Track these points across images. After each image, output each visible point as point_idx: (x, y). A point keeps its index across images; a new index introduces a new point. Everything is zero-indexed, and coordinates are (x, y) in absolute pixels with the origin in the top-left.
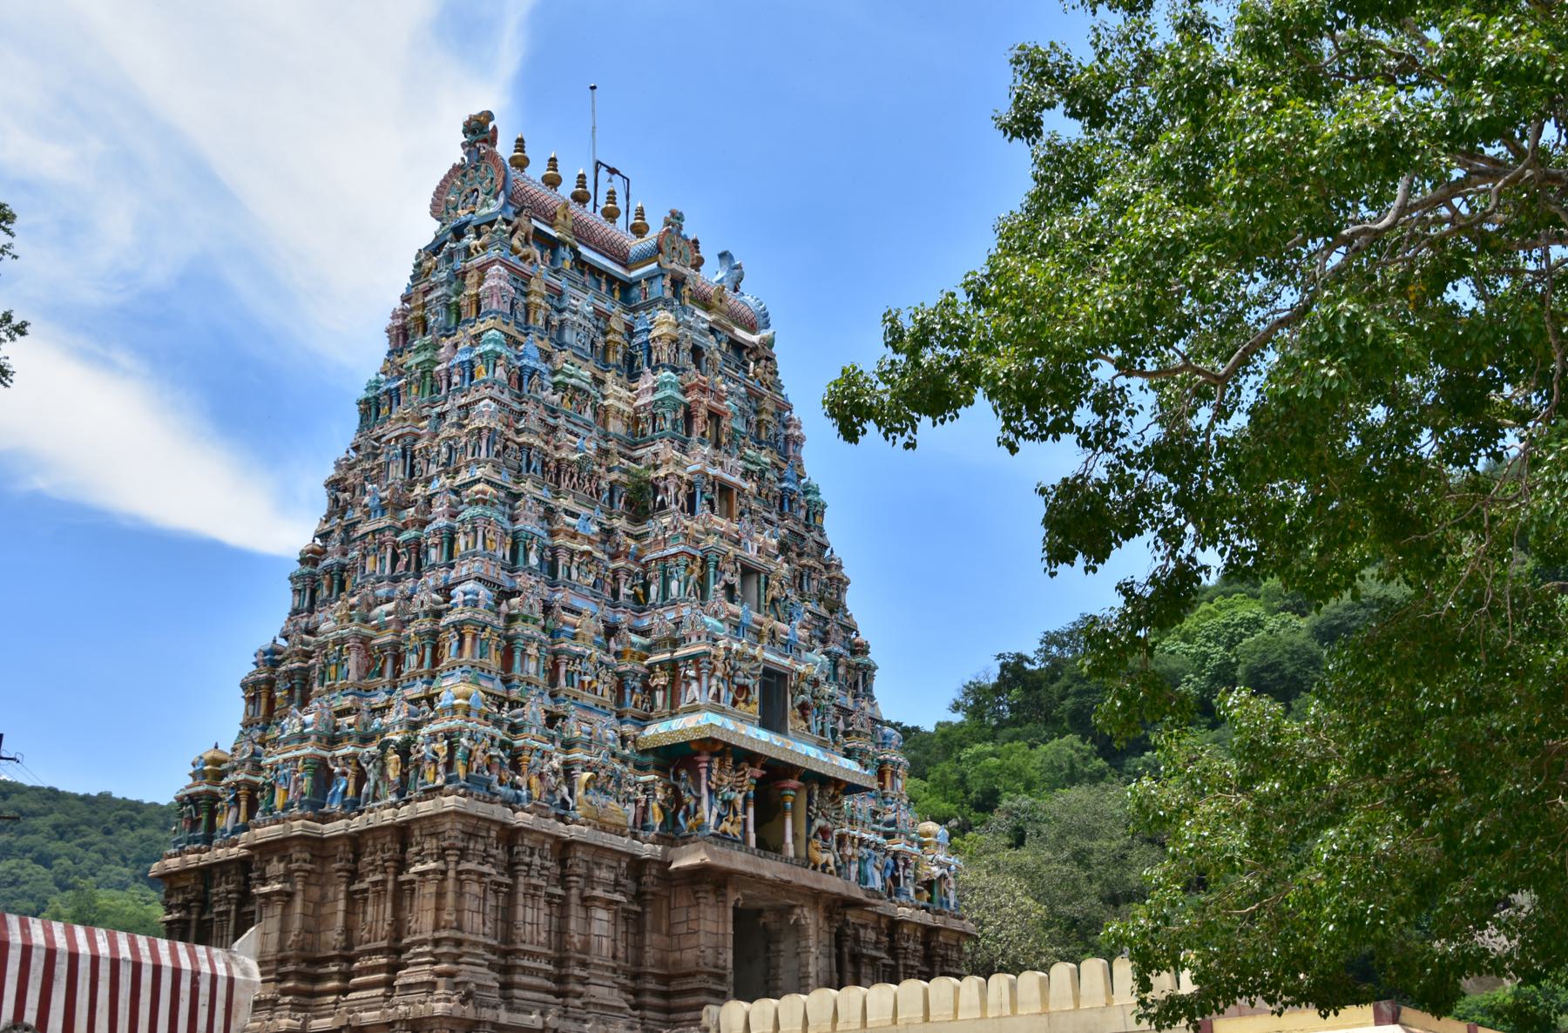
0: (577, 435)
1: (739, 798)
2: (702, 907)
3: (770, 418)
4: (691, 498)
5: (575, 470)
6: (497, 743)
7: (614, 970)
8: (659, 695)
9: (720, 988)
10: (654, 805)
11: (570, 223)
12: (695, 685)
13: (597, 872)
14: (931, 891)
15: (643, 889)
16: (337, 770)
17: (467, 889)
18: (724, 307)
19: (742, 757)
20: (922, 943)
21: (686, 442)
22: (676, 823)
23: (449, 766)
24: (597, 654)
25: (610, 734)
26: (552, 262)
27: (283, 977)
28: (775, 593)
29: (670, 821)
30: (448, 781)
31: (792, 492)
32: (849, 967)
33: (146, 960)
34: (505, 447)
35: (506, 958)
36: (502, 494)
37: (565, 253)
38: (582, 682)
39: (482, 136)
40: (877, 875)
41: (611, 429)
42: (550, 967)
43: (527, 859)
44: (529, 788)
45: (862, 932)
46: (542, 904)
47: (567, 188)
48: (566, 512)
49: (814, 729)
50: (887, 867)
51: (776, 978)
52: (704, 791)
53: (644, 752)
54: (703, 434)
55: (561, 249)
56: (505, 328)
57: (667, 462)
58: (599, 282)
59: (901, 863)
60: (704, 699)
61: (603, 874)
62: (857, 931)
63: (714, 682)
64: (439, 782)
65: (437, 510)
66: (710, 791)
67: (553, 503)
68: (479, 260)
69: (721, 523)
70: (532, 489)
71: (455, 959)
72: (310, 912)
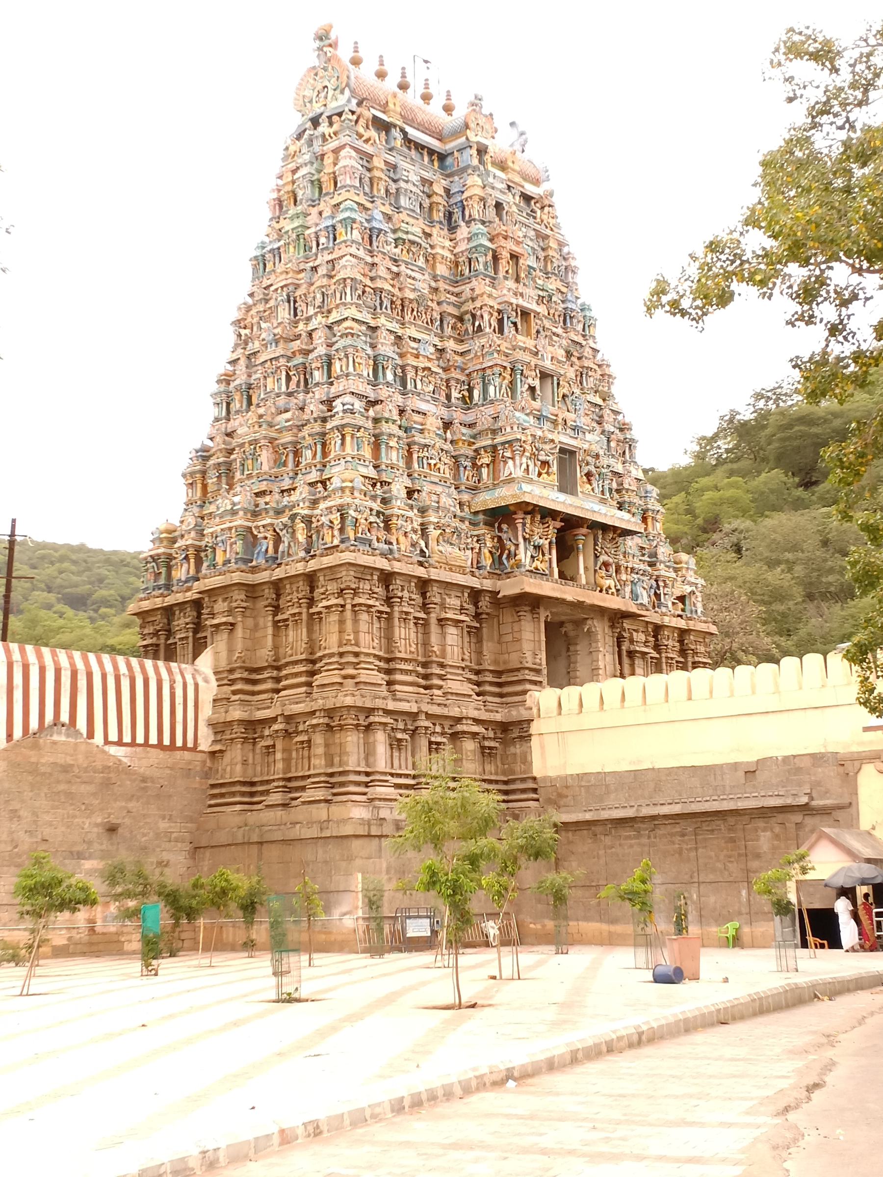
0: (414, 279)
2: (523, 623)
3: (555, 254)
4: (500, 322)
5: (415, 305)
6: (374, 513)
8: (485, 471)
10: (486, 551)
11: (398, 109)
12: (510, 462)
13: (448, 600)
16: (260, 536)
18: (517, 168)
19: (548, 514)
20: (679, 641)
23: (342, 530)
24: (439, 443)
28: (565, 391)
29: (498, 561)
30: (342, 541)
31: (572, 310)
32: (627, 660)
34: (364, 292)
36: (364, 328)
37: (396, 133)
43: (400, 594)
45: (635, 634)
49: (596, 491)
52: (521, 540)
53: (476, 513)
54: (507, 272)
55: (393, 130)
57: (482, 295)
58: (422, 154)
62: (631, 634)
63: (524, 460)
66: (525, 539)
67: (400, 332)
68: (333, 144)
69: (522, 340)
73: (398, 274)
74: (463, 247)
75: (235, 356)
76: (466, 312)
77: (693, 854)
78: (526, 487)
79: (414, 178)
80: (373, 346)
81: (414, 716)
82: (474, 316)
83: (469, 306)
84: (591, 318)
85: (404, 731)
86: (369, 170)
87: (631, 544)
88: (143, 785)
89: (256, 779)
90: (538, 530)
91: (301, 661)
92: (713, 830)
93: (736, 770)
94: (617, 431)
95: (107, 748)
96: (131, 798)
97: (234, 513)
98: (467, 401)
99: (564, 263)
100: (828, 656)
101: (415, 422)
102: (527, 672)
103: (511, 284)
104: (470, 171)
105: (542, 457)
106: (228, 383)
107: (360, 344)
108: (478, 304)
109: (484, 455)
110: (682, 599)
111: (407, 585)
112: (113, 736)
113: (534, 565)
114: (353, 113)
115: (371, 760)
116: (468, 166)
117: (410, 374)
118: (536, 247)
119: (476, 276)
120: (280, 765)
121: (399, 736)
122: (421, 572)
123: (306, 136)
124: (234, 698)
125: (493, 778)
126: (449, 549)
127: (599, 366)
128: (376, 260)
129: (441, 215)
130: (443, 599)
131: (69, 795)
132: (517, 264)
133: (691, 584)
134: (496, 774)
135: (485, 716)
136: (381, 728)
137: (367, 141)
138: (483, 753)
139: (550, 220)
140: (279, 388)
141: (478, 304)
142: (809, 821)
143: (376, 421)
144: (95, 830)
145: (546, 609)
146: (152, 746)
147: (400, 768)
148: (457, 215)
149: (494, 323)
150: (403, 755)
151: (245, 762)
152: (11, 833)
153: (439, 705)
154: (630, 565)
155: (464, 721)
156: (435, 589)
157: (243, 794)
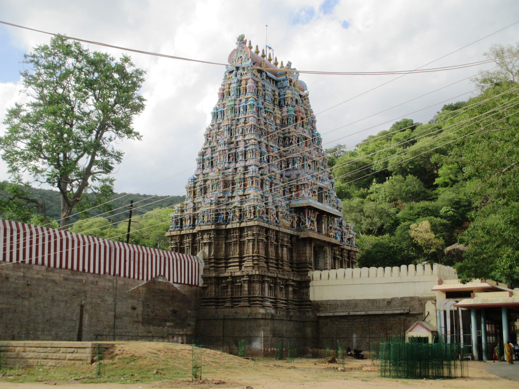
1: (314, 220)
19: (315, 210)
22: (299, 226)
23: (254, 213)
29: (298, 225)
30: (254, 217)
33: (70, 238)
35: (267, 260)
37: (264, 74)
47: (260, 54)
51: (318, 263)
52: (307, 219)
53: (291, 208)
61: (286, 239)
68: (244, 77)
71: (258, 260)
75: (206, 147)
76: (287, 137)
77: (368, 328)
79: (270, 90)
82: (289, 139)
83: (287, 135)
90: (313, 215)
91: (236, 258)
97: (211, 204)
100: (417, 266)
103: (301, 128)
105: (314, 190)
106: (203, 156)
110: (349, 239)
112: (175, 281)
122: (277, 229)
128: (260, 118)
135: (295, 279)
137: (256, 77)
140: (226, 160)
142: (409, 319)
143: (262, 175)
148: (282, 103)
151: (215, 291)
152: (147, 312)
157: (215, 302)
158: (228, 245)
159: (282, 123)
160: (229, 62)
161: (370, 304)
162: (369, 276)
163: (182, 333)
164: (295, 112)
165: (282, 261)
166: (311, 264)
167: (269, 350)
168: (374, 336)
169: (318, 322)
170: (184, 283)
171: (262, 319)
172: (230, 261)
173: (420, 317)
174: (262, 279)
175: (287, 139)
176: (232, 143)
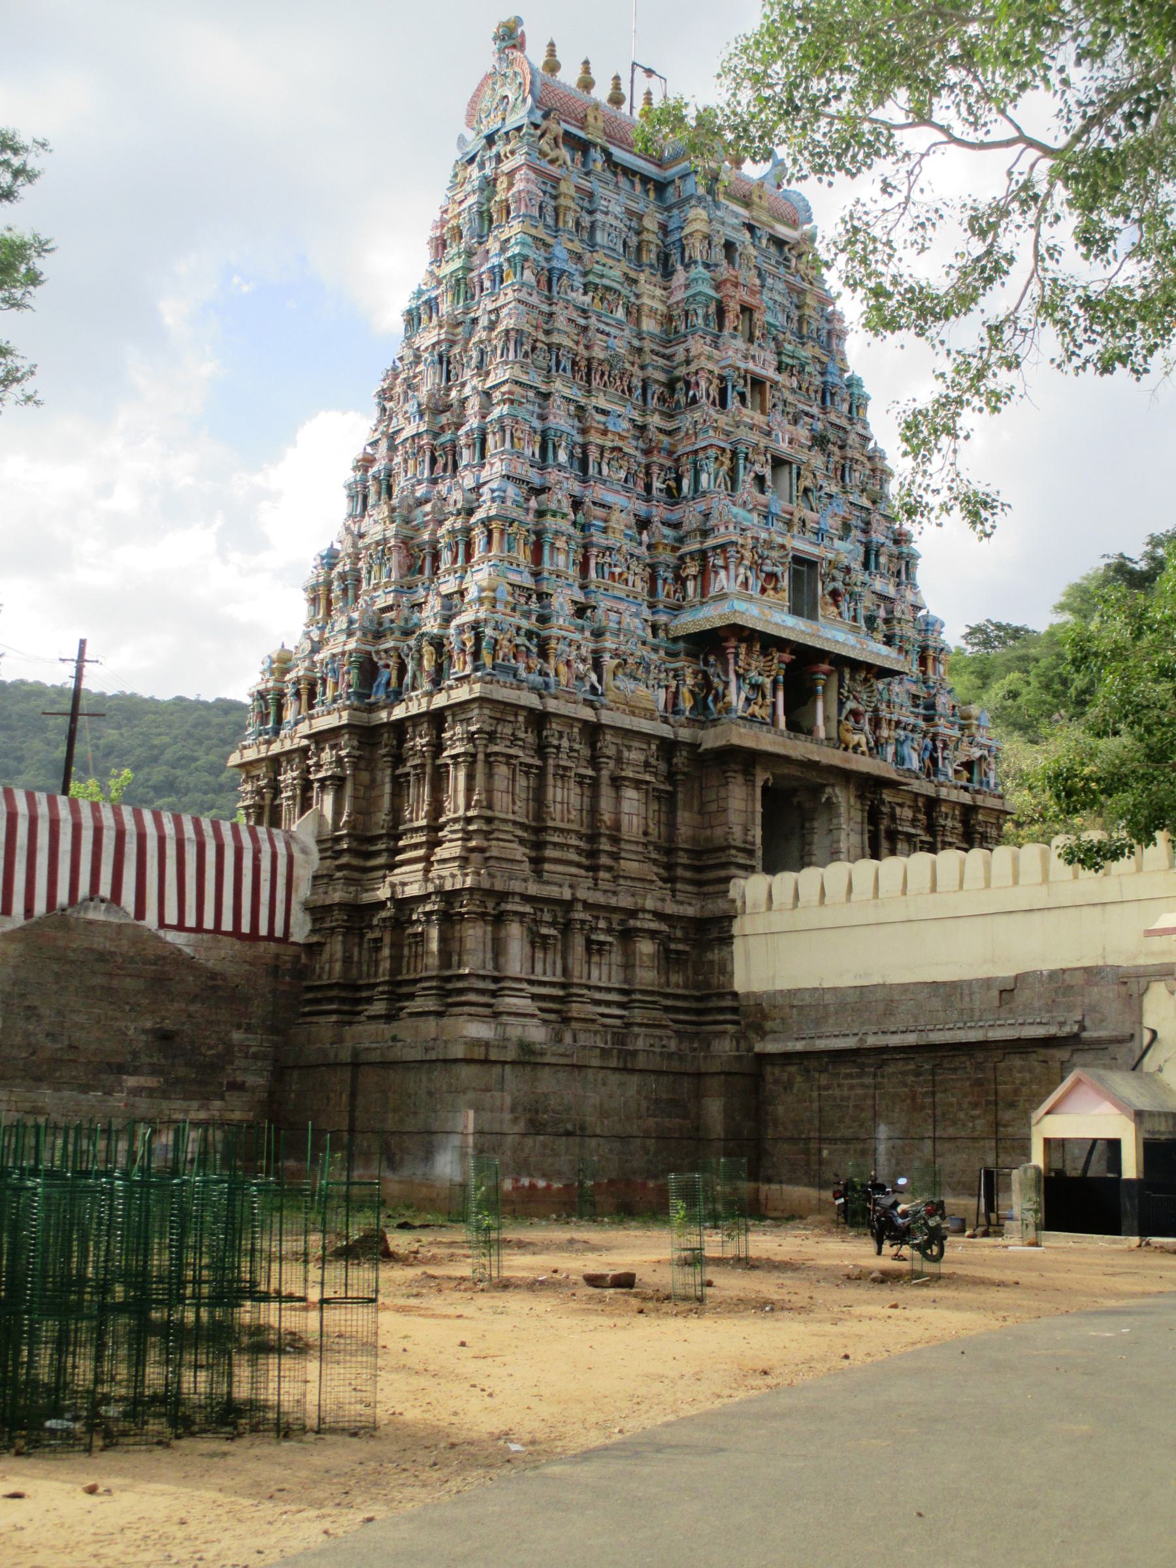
0: (608, 334)
1: (768, 682)
2: (731, 787)
3: (813, 313)
4: (723, 392)
5: (606, 368)
6: (522, 632)
7: (645, 845)
8: (690, 585)
9: (749, 862)
10: (684, 691)
11: (601, 124)
12: (723, 573)
13: (626, 754)
14: (971, 772)
15: (674, 769)
16: (381, 663)
17: (496, 770)
18: (764, 203)
19: (769, 643)
20: (961, 821)
21: (718, 337)
22: (706, 707)
23: (476, 655)
24: (628, 546)
25: (633, 624)
26: (584, 164)
27: (339, 854)
28: (808, 483)
29: (700, 705)
30: (476, 669)
31: (834, 385)
32: (881, 841)
34: (534, 349)
35: (537, 834)
36: (531, 394)
37: (596, 154)
38: (612, 574)
39: (512, 42)
40: (915, 756)
41: (645, 327)
42: (582, 844)
43: (556, 742)
44: (557, 674)
45: (898, 810)
46: (572, 785)
48: (597, 409)
49: (846, 615)
50: (926, 749)
52: (732, 677)
53: (675, 640)
54: (735, 329)
55: (592, 150)
56: (533, 232)
57: (698, 356)
58: (632, 182)
59: (940, 745)
60: (733, 587)
62: (893, 809)
63: (742, 570)
64: (468, 671)
65: (469, 412)
66: (738, 676)
67: (583, 401)
68: (506, 167)
69: (751, 415)
70: (561, 388)
71: (486, 835)
72: (361, 794)
73: (585, 329)
74: (679, 295)
76: (678, 379)
77: (928, 1100)
78: (740, 606)
79: (617, 210)
80: (543, 418)
81: (568, 905)
82: (688, 385)
83: (681, 371)
84: (861, 396)
85: (553, 924)
86: (555, 198)
87: (899, 690)
88: (210, 983)
89: (361, 982)
90: (758, 662)
92: (956, 1069)
93: (989, 988)
94: (890, 544)
95: (162, 933)
96: (194, 999)
98: (673, 495)
99: (827, 326)
101: (595, 518)
102: (733, 852)
103: (740, 343)
104: (693, 202)
107: (522, 413)
108: (693, 368)
109: (687, 564)
110: (969, 765)
111: (567, 730)
112: (171, 918)
113: (750, 710)
114: (536, 126)
115: (502, 960)
116: (691, 196)
117: (593, 454)
118: (786, 303)
119: (693, 334)
120: (386, 965)
121: (544, 931)
122: (588, 714)
123: (478, 159)
124: (339, 874)
125: (680, 991)
126: (630, 685)
127: (870, 458)
129: (653, 256)
130: (620, 752)
131: (109, 991)
132: (751, 320)
133: (981, 746)
134: (686, 987)
135: (670, 908)
136: (517, 918)
138: (667, 958)
139: (809, 271)
141: (693, 368)
144: (143, 1037)
145: (765, 770)
146: (226, 933)
147: (545, 973)
148: (675, 257)
149: (714, 392)
150: (550, 957)
152: (27, 1034)
153: (605, 891)
154: (895, 718)
155: (641, 915)
156: (608, 737)
157: (343, 1001)
158: (399, 785)
159: (667, 333)
160: (469, 124)
161: (937, 1003)
162: (934, 889)
163: (202, 1115)
164: (718, 287)
165: (615, 840)
166: (751, 853)
167: (508, 1185)
168: (951, 1131)
169: (757, 1077)
170: (199, 928)
171: (468, 1061)
172: (401, 843)
173: (1121, 1052)
174: (493, 908)
175: (680, 385)
176: (448, 407)
